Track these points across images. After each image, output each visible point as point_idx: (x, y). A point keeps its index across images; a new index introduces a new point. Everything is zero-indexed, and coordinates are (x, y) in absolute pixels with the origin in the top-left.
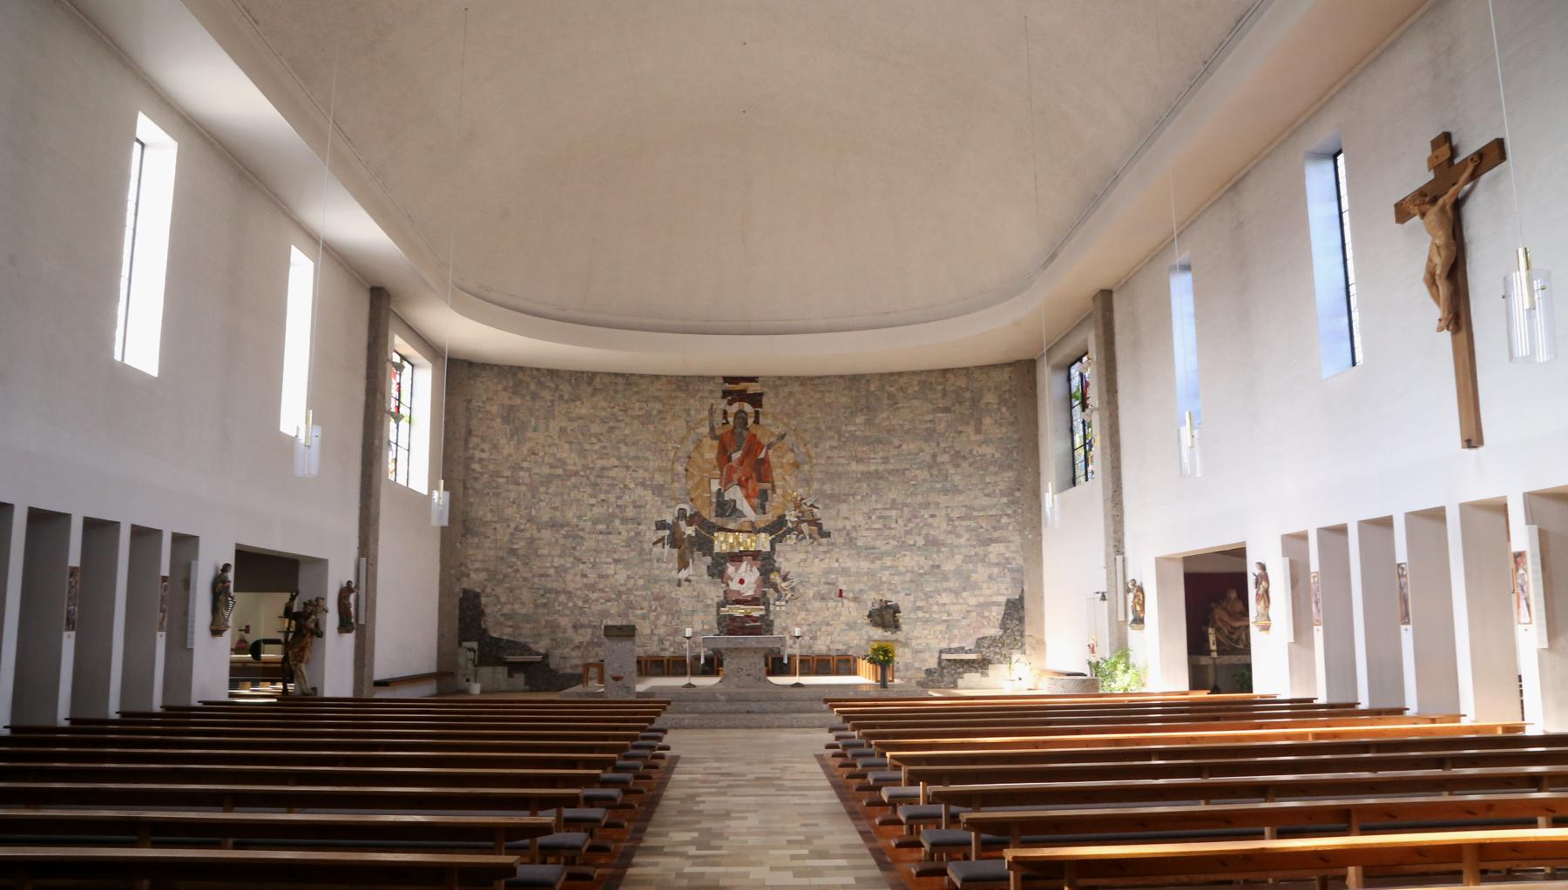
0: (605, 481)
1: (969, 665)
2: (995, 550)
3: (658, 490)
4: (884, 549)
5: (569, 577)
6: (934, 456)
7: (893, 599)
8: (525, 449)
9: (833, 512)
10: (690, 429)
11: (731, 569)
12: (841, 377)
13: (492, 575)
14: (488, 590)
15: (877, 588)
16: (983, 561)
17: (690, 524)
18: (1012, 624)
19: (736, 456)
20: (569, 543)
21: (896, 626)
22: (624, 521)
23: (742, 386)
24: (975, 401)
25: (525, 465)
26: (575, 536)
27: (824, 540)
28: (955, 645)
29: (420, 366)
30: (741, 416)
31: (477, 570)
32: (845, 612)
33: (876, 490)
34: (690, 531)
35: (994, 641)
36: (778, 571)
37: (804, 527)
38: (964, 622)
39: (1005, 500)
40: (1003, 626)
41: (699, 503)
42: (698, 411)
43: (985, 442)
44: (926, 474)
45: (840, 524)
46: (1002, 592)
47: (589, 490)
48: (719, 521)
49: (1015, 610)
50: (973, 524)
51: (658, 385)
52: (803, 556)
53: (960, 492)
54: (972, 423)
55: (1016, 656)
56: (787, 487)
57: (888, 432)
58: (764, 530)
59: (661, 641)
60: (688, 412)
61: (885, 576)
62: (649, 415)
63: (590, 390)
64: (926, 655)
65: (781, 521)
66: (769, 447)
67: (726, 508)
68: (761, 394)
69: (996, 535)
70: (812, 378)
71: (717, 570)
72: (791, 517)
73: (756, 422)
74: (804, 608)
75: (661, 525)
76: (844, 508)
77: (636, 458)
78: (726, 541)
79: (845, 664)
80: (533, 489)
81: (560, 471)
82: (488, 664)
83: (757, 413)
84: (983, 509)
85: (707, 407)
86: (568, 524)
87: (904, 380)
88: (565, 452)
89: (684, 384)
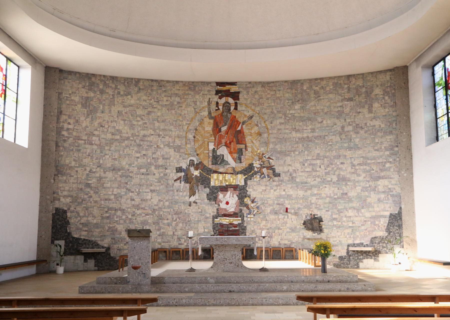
0: (145, 143)
1: (367, 254)
2: (382, 184)
3: (177, 149)
4: (312, 183)
5: (123, 200)
6: (343, 127)
7: (319, 214)
8: (96, 124)
9: (282, 162)
10: (196, 113)
11: (221, 196)
12: (286, 82)
13: (75, 200)
14: (72, 209)
15: (308, 207)
17: (196, 169)
18: (394, 229)
19: (224, 129)
20: (123, 180)
21: (320, 230)
22: (157, 167)
23: (228, 87)
24: (368, 94)
25: (96, 133)
26: (127, 176)
27: (276, 179)
28: (357, 242)
29: (24, 67)
31: (65, 197)
32: (289, 221)
34: (196, 173)
35: (382, 239)
36: (249, 197)
37: (265, 170)
38: (363, 228)
39: (388, 153)
40: (388, 230)
41: (202, 156)
42: (201, 102)
43: (375, 118)
44: (338, 138)
45: (286, 169)
46: (388, 209)
47: (136, 149)
48: (214, 167)
49: (396, 221)
50: (368, 168)
51: (177, 87)
52: (264, 188)
53: (359, 148)
54: (367, 107)
55: (397, 249)
56: (254, 147)
57: (315, 114)
58: (241, 172)
59: (179, 239)
60: (195, 102)
61: (314, 199)
62: (172, 104)
63: (136, 89)
64: (340, 248)
65: (251, 167)
66: (244, 123)
67: (217, 160)
68: (239, 93)
69: (382, 174)
70: (268, 83)
71: (213, 196)
72: (257, 165)
73: (236, 109)
74: (264, 219)
75: (179, 170)
76: (288, 159)
77: (164, 130)
78: (218, 179)
79: (290, 253)
80: (100, 146)
81: (118, 137)
82: (71, 254)
83: (236, 104)
84: (374, 158)
85: (207, 100)
86: (123, 169)
87: (324, 82)
89: (193, 86)
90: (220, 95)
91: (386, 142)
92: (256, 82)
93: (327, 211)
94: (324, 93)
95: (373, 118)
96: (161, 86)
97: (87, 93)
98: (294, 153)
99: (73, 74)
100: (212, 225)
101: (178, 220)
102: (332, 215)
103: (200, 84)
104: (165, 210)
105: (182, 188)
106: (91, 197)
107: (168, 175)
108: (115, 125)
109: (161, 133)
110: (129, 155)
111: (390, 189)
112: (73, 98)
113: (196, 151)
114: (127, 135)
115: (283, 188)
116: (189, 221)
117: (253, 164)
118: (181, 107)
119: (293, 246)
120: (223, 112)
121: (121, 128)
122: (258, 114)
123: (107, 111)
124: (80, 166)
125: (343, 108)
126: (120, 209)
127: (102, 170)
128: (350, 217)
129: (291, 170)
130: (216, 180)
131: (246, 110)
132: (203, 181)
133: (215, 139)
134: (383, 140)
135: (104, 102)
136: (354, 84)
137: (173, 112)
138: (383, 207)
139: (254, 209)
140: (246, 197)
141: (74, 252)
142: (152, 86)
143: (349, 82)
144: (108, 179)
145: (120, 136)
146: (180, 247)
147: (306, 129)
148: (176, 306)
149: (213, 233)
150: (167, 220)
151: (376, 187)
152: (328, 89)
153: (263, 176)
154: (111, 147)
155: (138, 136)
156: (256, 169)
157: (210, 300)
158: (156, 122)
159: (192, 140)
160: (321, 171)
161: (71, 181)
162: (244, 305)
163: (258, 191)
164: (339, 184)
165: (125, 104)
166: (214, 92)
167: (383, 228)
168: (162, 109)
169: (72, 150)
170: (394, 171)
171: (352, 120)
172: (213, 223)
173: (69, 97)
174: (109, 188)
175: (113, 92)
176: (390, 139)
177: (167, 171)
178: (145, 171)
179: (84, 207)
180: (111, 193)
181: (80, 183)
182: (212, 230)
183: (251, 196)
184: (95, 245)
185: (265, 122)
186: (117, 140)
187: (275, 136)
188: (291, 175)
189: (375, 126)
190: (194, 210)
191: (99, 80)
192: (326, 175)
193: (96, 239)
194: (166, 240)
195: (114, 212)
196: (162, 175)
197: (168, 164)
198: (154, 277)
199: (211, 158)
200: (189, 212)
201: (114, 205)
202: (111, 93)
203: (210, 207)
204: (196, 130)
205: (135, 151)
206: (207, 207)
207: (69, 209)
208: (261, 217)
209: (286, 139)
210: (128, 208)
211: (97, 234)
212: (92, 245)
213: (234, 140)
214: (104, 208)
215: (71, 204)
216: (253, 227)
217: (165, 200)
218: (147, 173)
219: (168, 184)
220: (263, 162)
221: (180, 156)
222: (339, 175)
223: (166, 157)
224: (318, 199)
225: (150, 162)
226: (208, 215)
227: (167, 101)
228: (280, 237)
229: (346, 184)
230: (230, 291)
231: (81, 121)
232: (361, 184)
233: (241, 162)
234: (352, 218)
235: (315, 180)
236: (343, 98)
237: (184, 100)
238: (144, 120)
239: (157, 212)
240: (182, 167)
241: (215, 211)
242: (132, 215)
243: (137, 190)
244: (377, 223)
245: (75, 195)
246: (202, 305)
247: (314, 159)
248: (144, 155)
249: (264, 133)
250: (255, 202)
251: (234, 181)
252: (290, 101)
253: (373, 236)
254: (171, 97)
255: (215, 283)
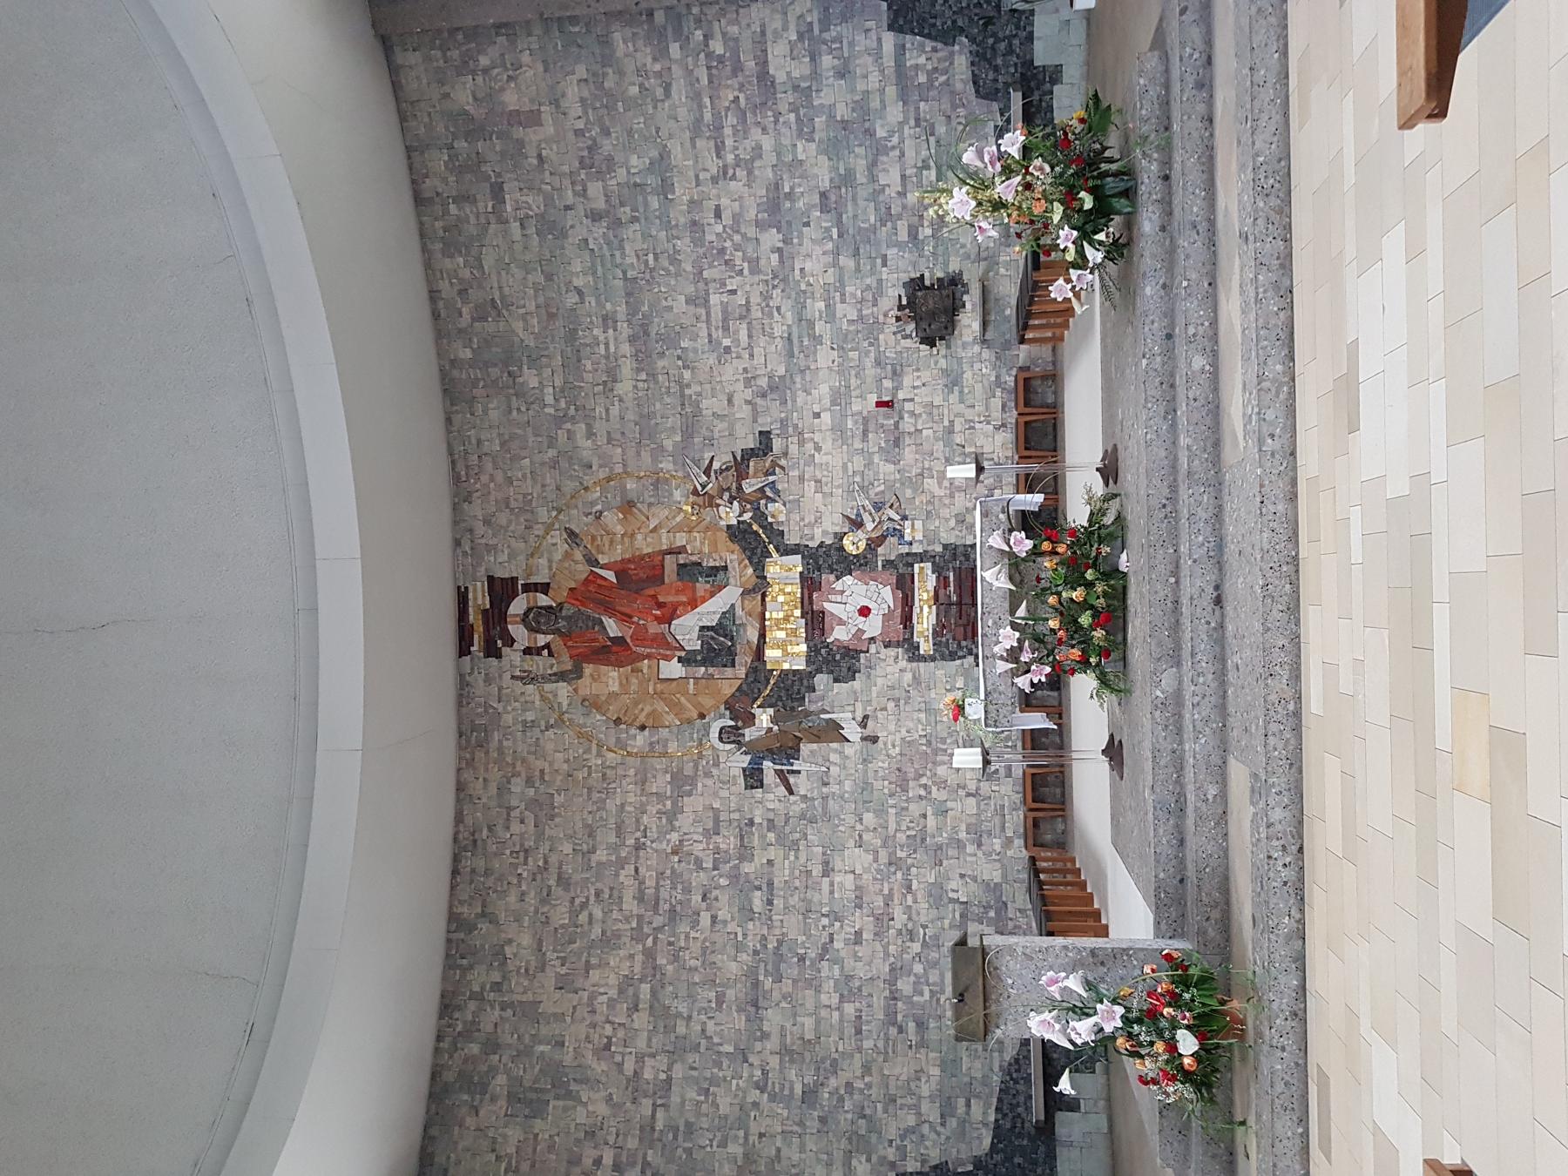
0: (664, 894)
2: (783, 65)
3: (682, 784)
5: (861, 971)
6: (595, 216)
7: (894, 292)
8: (599, 1067)
10: (560, 722)
11: (839, 634)
14: (891, 1154)
15: (872, 329)
16: (807, 93)
17: (750, 719)
19: (613, 627)
21: (954, 283)
22: (745, 853)
24: (473, 129)
25: (629, 1067)
27: (777, 445)
30: (533, 620)
32: (923, 396)
33: (671, 339)
34: (764, 718)
36: (840, 537)
37: (750, 486)
38: (941, 130)
39: (675, 49)
41: (707, 702)
43: (556, 103)
45: (744, 412)
47: (683, 928)
48: (744, 660)
51: (477, 788)
52: (810, 487)
53: (664, 155)
54: (518, 132)
56: (674, 524)
57: (552, 316)
58: (759, 569)
60: (527, 726)
61: (846, 311)
62: (533, 804)
63: (484, 926)
65: (738, 534)
66: (596, 563)
67: (717, 647)
68: (491, 579)
70: (456, 479)
71: (841, 662)
72: (730, 514)
73: (545, 588)
75: (753, 777)
76: (710, 405)
78: (782, 645)
80: (677, 1051)
81: (645, 988)
83: (527, 588)
87: (444, 285)
88: (605, 981)
89: (473, 734)
90: (499, 643)
91: (638, 55)
92: (455, 523)
93: (884, 264)
94: (480, 286)
95: (558, 106)
96: (475, 841)
97: (493, 1099)
98: (688, 386)
99: (430, 1150)
100: (940, 663)
101: (924, 781)
102: (898, 245)
103: (464, 710)
104: (892, 826)
105: (814, 768)
106: (849, 1085)
107: (771, 815)
108: (604, 998)
109: (631, 842)
110: (704, 949)
111: (801, 36)
112: (511, 1150)
113: (690, 722)
114: (639, 958)
115: (808, 419)
116: (929, 743)
117: (729, 527)
118: (542, 771)
119: (1010, 381)
120: (557, 632)
121: (613, 980)
122: (560, 511)
123: (556, 1028)
124: (742, 1123)
125: (528, 216)
126: (892, 982)
127: (758, 1046)
128: (903, 177)
129: (748, 394)
130: (787, 651)
131: (550, 553)
132: (790, 697)
133: (649, 656)
134: (630, 67)
135: (527, 1039)
136: (445, 180)
137: (558, 800)
138: (870, 60)
139: (884, 518)
140: (842, 549)
141: (1042, 1149)
142: (473, 871)
143: (437, 199)
144: (788, 1025)
145: (641, 981)
146: (1018, 771)
147: (607, 345)
148: (1301, 850)
149: (971, 659)
150: (925, 816)
151: (796, 88)
152: (466, 274)
153: (769, 493)
154: (679, 1015)
155: (640, 917)
156: (747, 516)
157: (1273, 698)
158: (595, 858)
159: (651, 736)
160: (748, 288)
161: (796, 1157)
162: (1294, 538)
163: (822, 508)
164: (789, 223)
165: (533, 964)
166: (493, 661)
167: (940, 54)
168: (551, 838)
169: (689, 1151)
170: (736, 22)
171: (567, 182)
172: (933, 659)
173: (509, 1163)
174: (818, 1022)
175: (493, 1008)
176: (625, 42)
177: (757, 820)
178: (758, 893)
179: (886, 1111)
180: (836, 1014)
181: (801, 1124)
182: (958, 662)
183: (838, 529)
184: (1018, 1071)
185: (586, 489)
186: (654, 993)
187: (631, 453)
188: (764, 396)
189: (582, 100)
190: (892, 727)
191: (451, 1057)
192: (759, 272)
193: (996, 1069)
194: (997, 820)
195: (900, 1004)
196: (771, 836)
197: (736, 816)
198: (1157, 923)
199: (711, 670)
200: (898, 742)
201: (878, 1002)
202: (497, 1013)
203: (879, 671)
204: (618, 722)
205: (692, 928)
206: (880, 681)
207: (893, 1165)
208: (909, 493)
209: (642, 416)
210: (886, 954)
211: (977, 1064)
212: (1016, 1082)
213: (651, 592)
214: (887, 1040)
215: (874, 1158)
216: (947, 520)
217: (859, 827)
218: (764, 887)
219: (802, 816)
220: (722, 490)
221: (708, 775)
222: (758, 224)
223: (710, 825)
224: (843, 295)
225: (729, 877)
226: (908, 677)
227: (522, 822)
228: (978, 426)
229: (790, 196)
230: (1218, 601)
231: (591, 1121)
232: (786, 141)
233: (725, 568)
234: (908, 172)
235: (778, 309)
236: (492, 219)
237: (519, 763)
238: (588, 898)
239: (900, 854)
240: (744, 770)
241: (892, 652)
242: (912, 940)
243: (825, 921)
244: (922, 78)
245: (844, 1144)
246: (1297, 730)
247: (708, 314)
248: (704, 898)
249: (624, 490)
250: (858, 515)
251: (789, 589)
252: (514, 402)
253: (971, 89)
254: (510, 809)
255: (1178, 664)
